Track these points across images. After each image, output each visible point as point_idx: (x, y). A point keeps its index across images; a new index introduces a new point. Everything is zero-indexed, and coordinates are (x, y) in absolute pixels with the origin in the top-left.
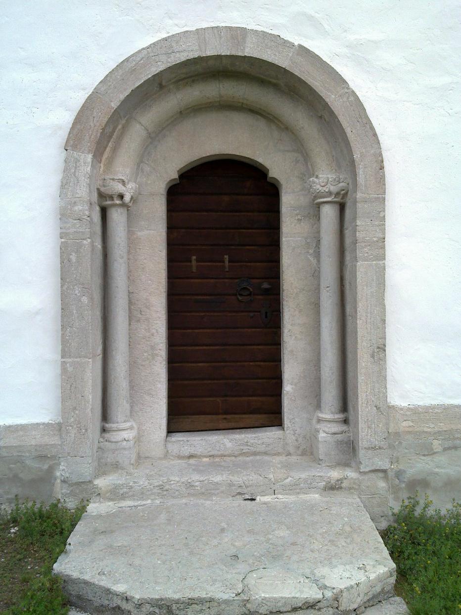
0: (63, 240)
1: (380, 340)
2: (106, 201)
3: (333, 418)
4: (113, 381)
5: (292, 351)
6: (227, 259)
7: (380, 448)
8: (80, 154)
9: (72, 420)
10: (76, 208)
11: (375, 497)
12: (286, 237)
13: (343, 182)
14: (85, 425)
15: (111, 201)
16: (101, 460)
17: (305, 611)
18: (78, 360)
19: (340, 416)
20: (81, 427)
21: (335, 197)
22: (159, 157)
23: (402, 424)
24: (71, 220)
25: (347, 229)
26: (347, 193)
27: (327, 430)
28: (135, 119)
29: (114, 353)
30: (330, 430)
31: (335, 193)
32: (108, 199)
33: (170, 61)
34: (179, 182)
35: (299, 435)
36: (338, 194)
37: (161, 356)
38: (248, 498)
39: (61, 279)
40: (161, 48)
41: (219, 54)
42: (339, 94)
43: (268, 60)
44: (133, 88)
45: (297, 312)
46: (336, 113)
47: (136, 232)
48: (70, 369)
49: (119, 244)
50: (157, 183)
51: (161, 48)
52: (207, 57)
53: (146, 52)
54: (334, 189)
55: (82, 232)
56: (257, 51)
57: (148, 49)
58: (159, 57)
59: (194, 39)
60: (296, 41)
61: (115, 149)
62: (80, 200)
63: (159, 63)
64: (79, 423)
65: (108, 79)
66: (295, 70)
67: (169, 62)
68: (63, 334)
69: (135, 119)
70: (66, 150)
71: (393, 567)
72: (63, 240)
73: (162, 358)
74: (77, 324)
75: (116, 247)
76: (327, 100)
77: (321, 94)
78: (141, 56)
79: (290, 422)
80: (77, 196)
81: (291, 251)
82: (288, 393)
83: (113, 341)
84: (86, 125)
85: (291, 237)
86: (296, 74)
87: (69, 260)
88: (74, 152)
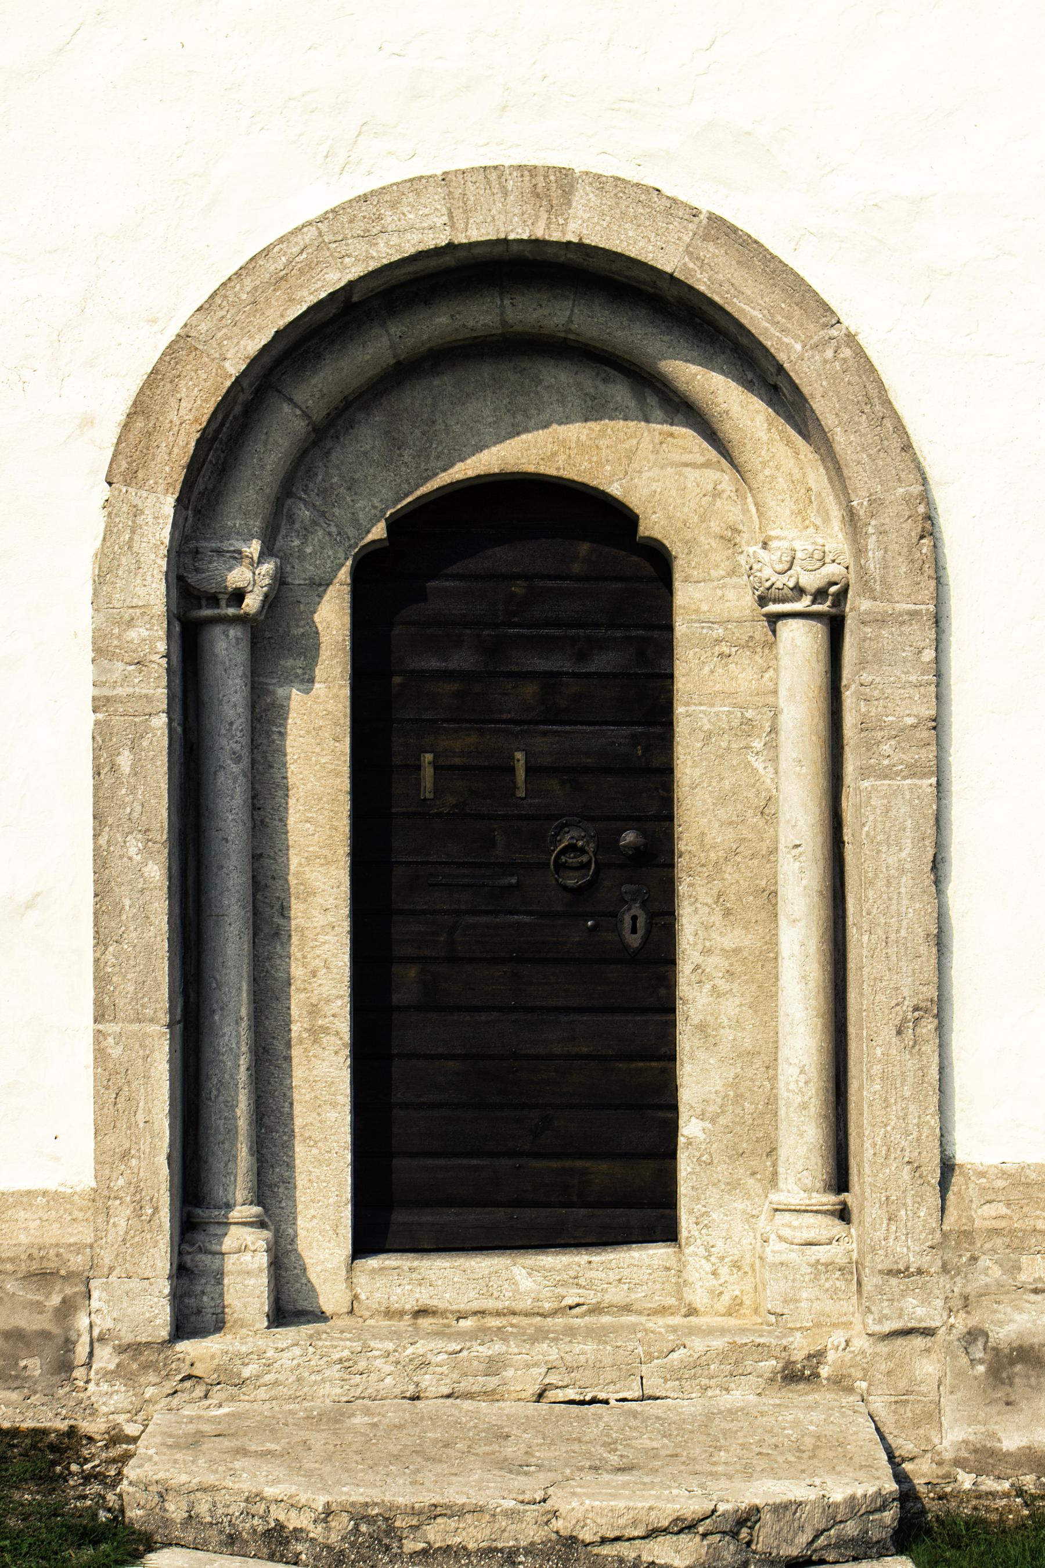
0: (100, 716)
1: (925, 989)
2: (200, 607)
3: (808, 1202)
4: (214, 1093)
5: (702, 1027)
6: (522, 762)
7: (920, 1272)
8: (145, 494)
9: (121, 1182)
10: (133, 634)
11: (907, 1401)
12: (687, 704)
13: (833, 561)
14: (152, 1199)
15: (213, 608)
16: (187, 1301)
17: (675, 1538)
18: (136, 1027)
19: (830, 1200)
20: (144, 1203)
21: (813, 602)
22: (335, 480)
23: (979, 1212)
24: (120, 665)
25: (847, 687)
26: (845, 590)
27: (787, 1233)
28: (280, 392)
29: (217, 1018)
30: (798, 1234)
31: (813, 591)
32: (204, 602)
33: (375, 254)
34: (387, 544)
35: (722, 1258)
36: (820, 594)
37: (337, 1033)
38: (572, 1397)
39: (95, 817)
40: (351, 222)
41: (502, 236)
42: (812, 342)
43: (627, 253)
44: (282, 323)
45: (717, 918)
46: (806, 390)
47: (271, 688)
48: (116, 1052)
49: (231, 724)
50: (330, 553)
51: (351, 222)
52: (470, 244)
53: (316, 233)
54: (811, 581)
55: (146, 696)
56: (599, 228)
57: (320, 224)
58: (347, 245)
59: (436, 197)
60: (705, 205)
61: (224, 470)
62: (143, 614)
63: (347, 260)
64: (138, 1190)
65: (218, 300)
66: (698, 280)
67: (373, 258)
68: (97, 961)
69: (280, 392)
70: (110, 484)
71: (893, 1489)
72: (100, 716)
73: (341, 1039)
74: (134, 935)
75: (223, 732)
76: (782, 357)
77: (765, 342)
78: (301, 240)
79: (697, 1224)
80: (135, 602)
81: (699, 745)
82: (690, 1144)
83: (214, 985)
84: (161, 419)
85: (701, 704)
86: (702, 288)
87: (114, 768)
88: (130, 489)
